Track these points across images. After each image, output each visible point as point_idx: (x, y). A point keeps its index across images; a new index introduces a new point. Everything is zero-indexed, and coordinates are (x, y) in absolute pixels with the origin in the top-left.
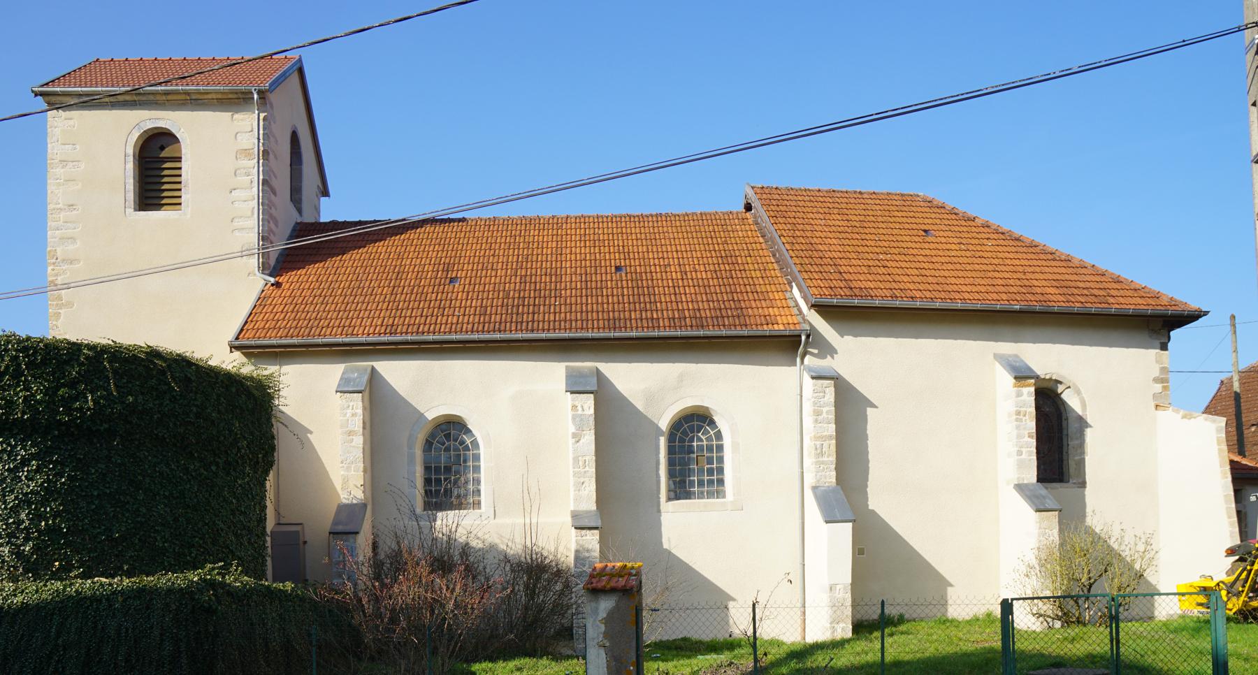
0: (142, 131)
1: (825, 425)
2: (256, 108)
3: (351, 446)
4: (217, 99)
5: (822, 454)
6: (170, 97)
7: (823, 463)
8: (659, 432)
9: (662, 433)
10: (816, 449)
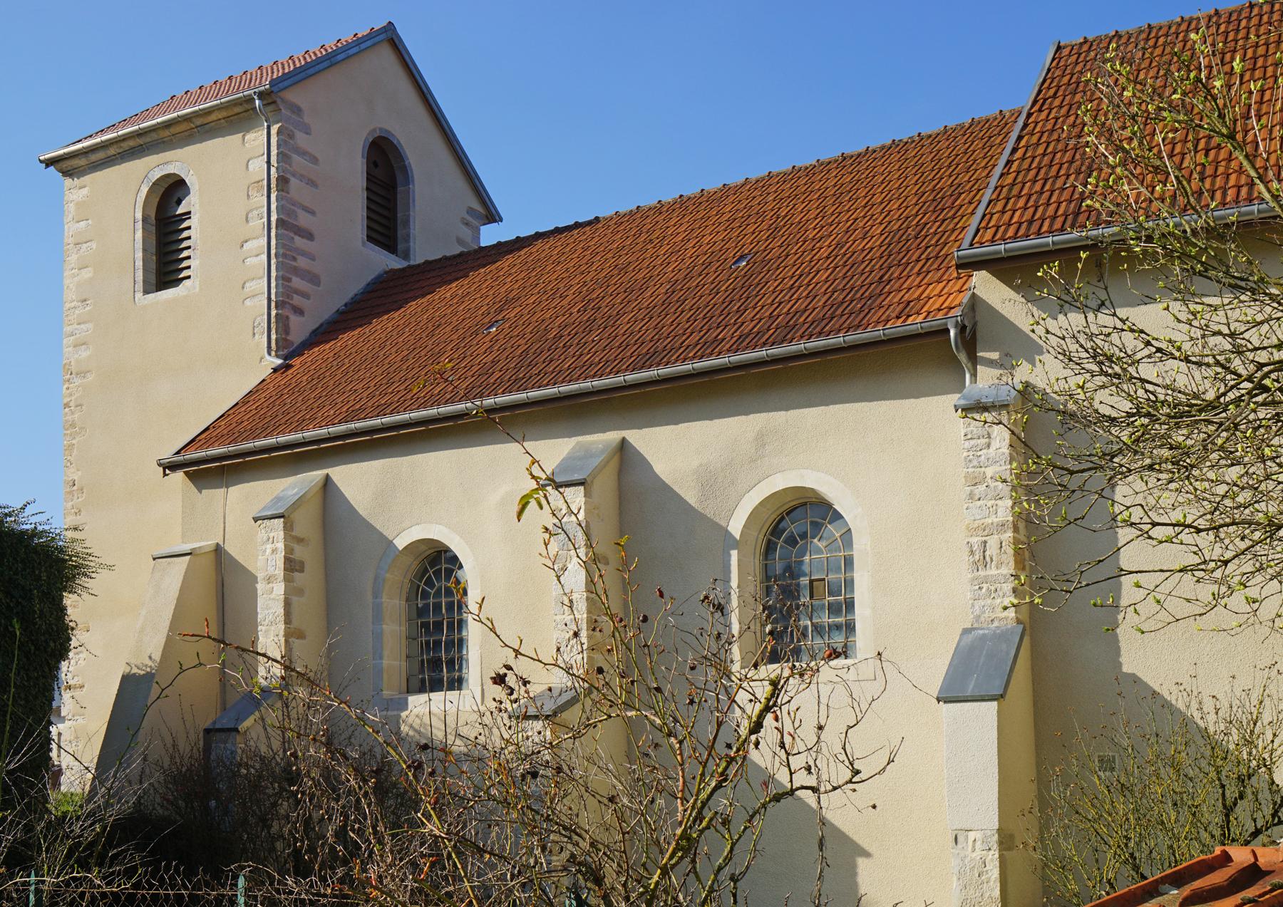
0: (151, 184)
1: (990, 503)
2: (264, 118)
3: (270, 599)
4: (224, 118)
5: (984, 562)
6: (174, 130)
7: (986, 580)
8: (728, 541)
9: (735, 544)
10: (972, 552)
